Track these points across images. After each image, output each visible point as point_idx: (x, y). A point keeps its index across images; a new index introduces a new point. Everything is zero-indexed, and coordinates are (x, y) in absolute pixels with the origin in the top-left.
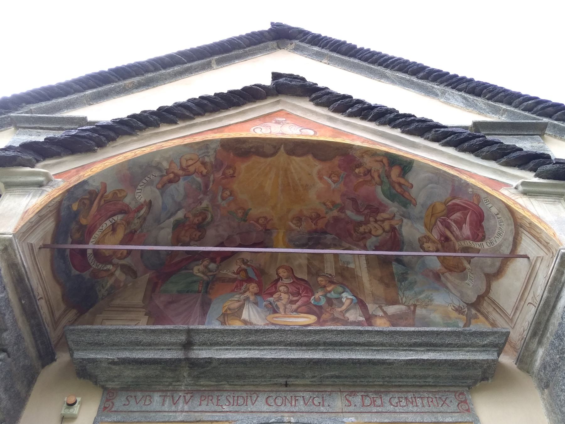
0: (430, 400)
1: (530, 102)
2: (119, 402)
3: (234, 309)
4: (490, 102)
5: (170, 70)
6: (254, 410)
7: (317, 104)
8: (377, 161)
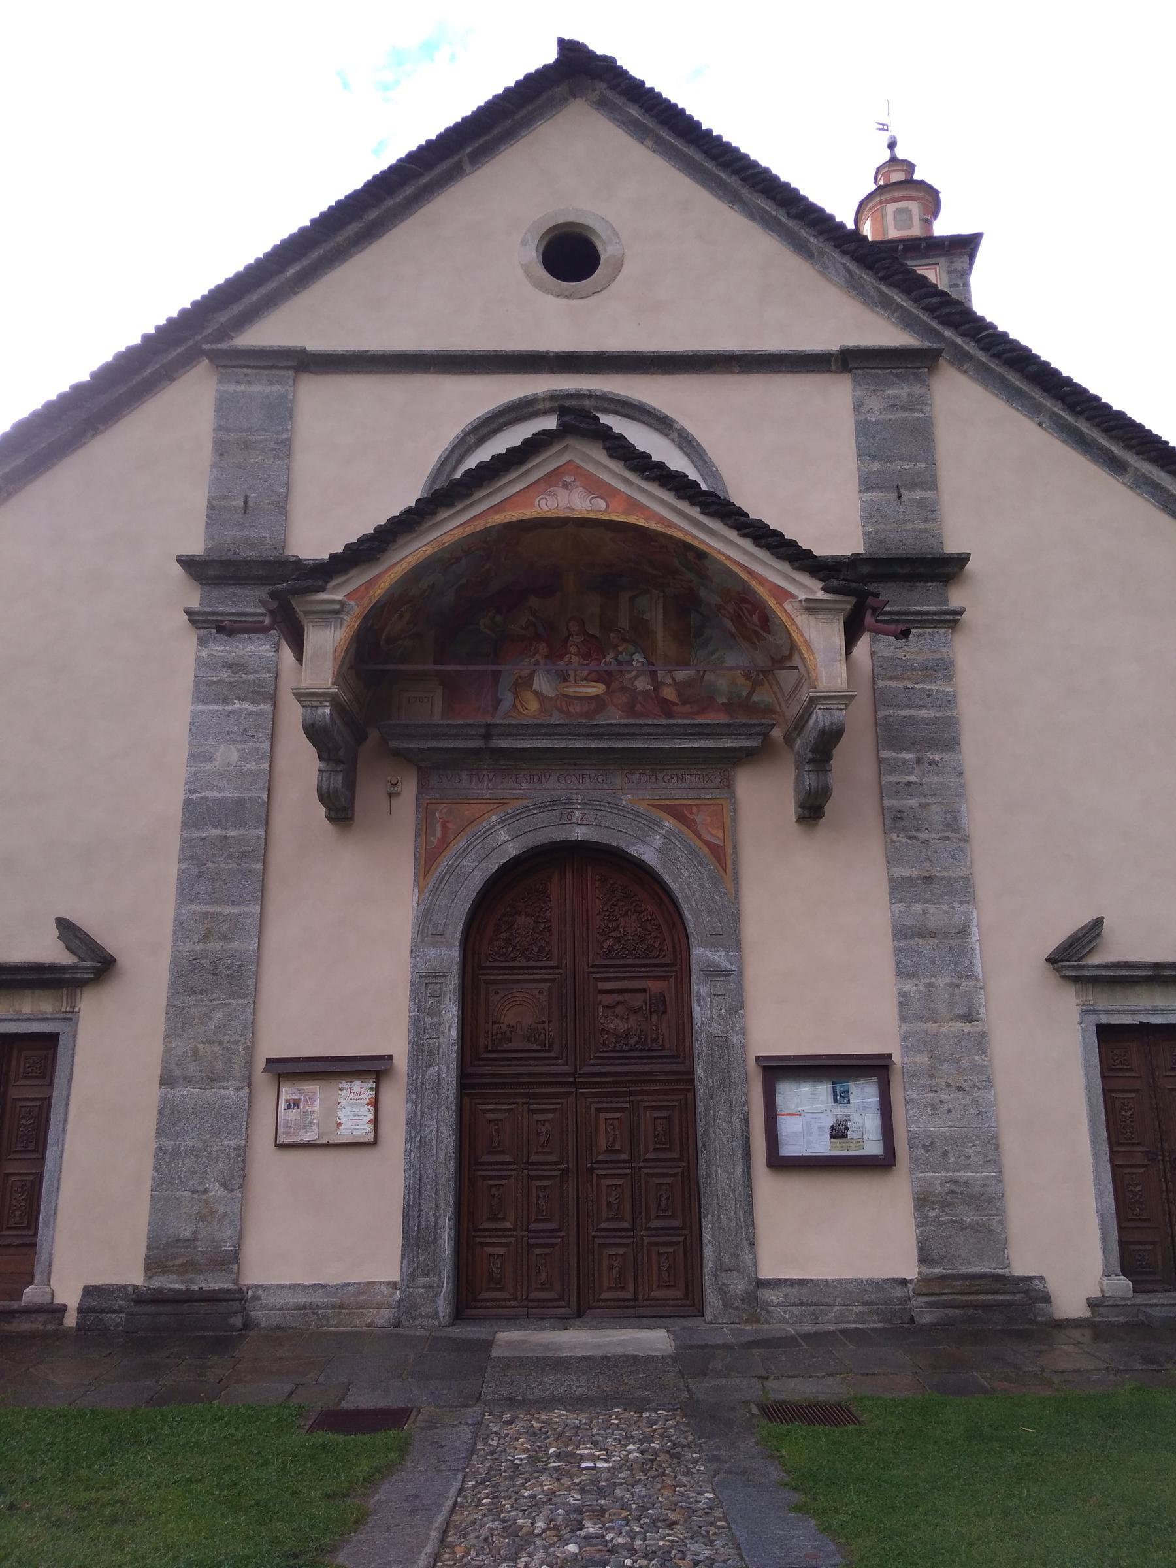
4: (883, 288)
5: (400, 197)
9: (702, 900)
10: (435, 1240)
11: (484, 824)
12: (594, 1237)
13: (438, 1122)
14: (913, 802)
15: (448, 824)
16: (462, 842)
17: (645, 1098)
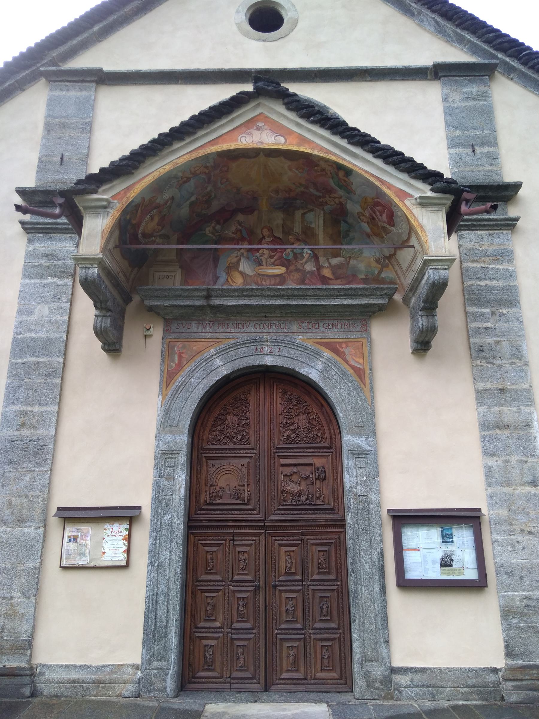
0: (346, 324)
1: (491, 35)
2: (174, 327)
3: (234, 263)
4: (459, 31)
6: (248, 331)
7: (288, 109)
8: (329, 165)
10: (166, 636)
11: (206, 354)
12: (277, 634)
13: (170, 552)
14: (490, 340)
17: (312, 537)
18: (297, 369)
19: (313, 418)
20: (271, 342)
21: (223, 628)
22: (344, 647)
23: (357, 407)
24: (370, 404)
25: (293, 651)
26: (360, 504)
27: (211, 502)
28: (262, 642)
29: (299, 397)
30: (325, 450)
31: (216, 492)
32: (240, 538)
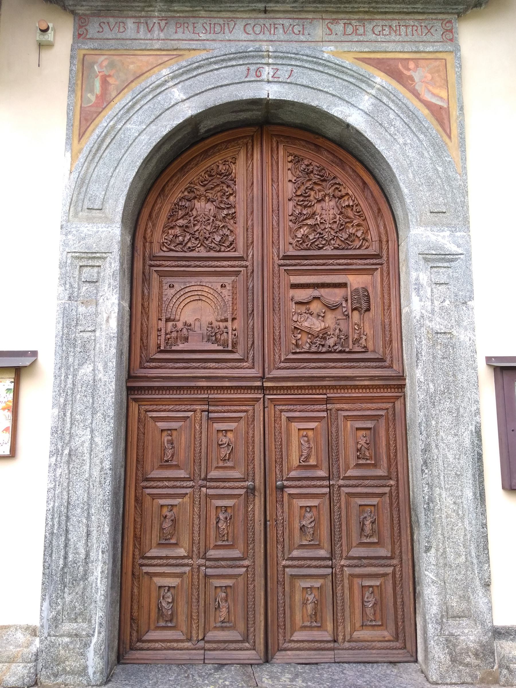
0: (415, 28)
2: (93, 29)
6: (232, 38)
9: (420, 171)
10: (85, 577)
11: (153, 78)
12: (285, 567)
13: (92, 431)
15: (108, 79)
16: (126, 99)
17: (345, 406)
18: (325, 108)
19: (348, 206)
20: (276, 57)
21: (192, 558)
22: (402, 587)
23: (434, 177)
24: (460, 170)
25: (313, 596)
26: (439, 347)
27: (168, 348)
28: (260, 581)
29: (323, 169)
30: (368, 261)
31: (177, 332)
32: (219, 408)
